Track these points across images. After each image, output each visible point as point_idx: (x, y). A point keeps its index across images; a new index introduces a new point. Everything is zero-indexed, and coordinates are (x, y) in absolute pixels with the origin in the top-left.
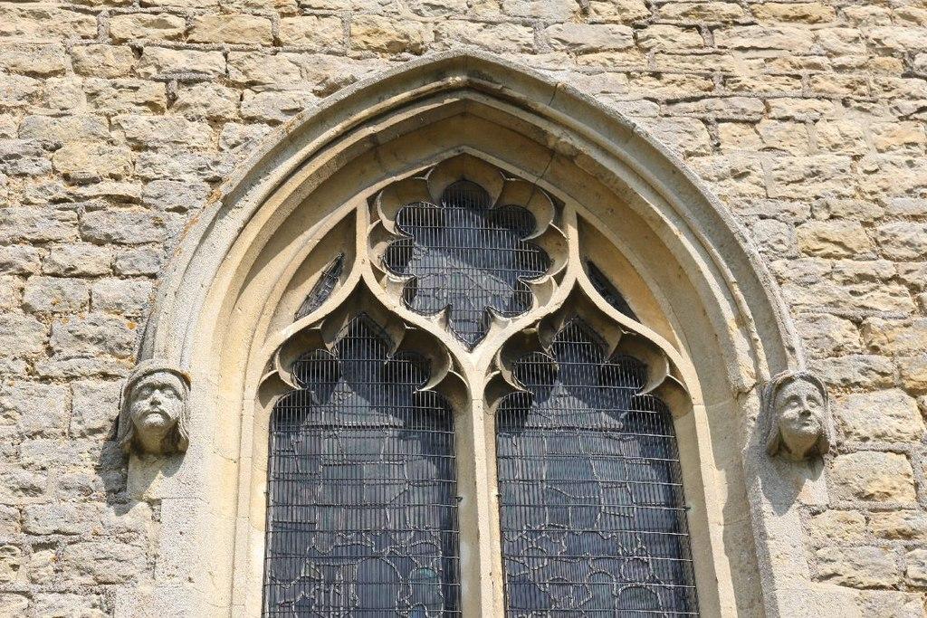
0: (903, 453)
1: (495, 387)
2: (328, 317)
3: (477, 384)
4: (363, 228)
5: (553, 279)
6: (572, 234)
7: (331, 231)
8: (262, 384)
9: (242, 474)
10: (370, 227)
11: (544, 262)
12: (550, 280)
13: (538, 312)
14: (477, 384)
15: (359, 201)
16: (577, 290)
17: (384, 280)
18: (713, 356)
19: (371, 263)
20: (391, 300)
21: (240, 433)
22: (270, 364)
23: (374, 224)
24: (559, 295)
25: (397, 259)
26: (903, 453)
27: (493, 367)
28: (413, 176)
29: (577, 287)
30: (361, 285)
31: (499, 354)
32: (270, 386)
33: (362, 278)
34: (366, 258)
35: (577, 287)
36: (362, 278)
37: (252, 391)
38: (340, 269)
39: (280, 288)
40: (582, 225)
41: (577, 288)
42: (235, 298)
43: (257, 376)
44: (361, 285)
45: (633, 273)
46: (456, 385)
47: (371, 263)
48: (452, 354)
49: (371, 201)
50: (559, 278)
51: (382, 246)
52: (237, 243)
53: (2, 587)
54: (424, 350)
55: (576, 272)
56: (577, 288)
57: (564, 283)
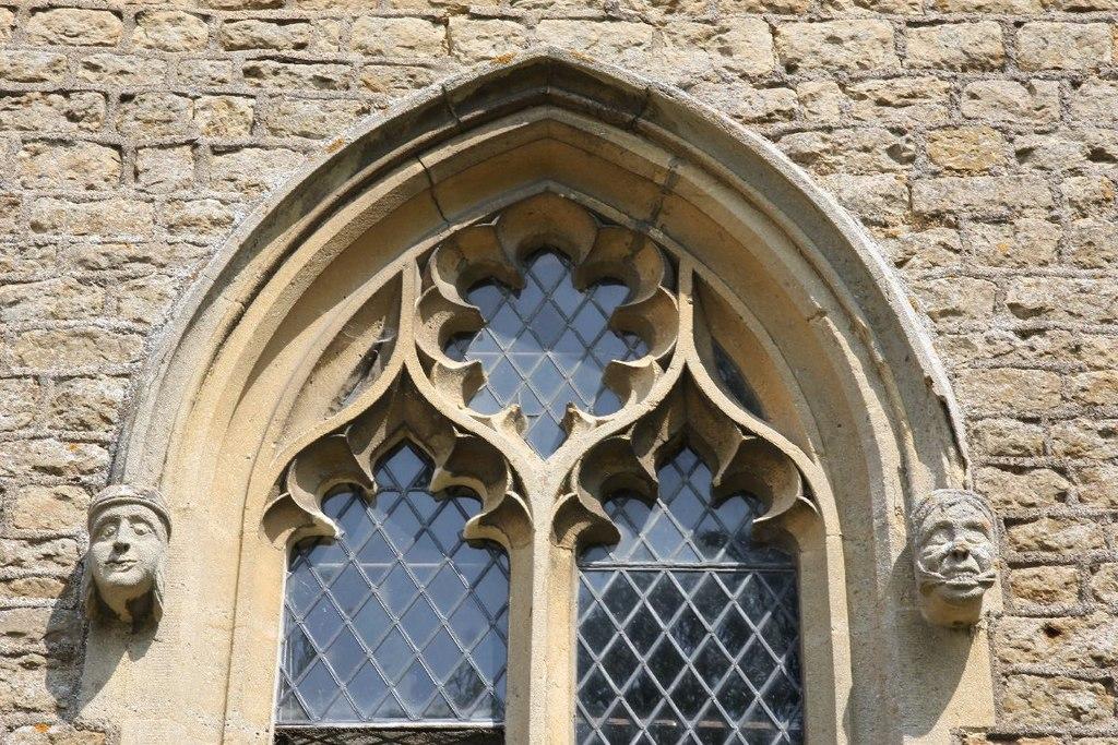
0: (1034, 577)
1: (569, 513)
3: (543, 509)
6: (685, 307)
7: (361, 310)
9: (222, 701)
14: (543, 509)
15: (406, 261)
19: (417, 348)
20: (445, 398)
21: (241, 542)
22: (282, 483)
24: (663, 385)
25: (456, 337)
26: (1034, 577)
27: (566, 487)
29: (686, 373)
30: (404, 376)
32: (281, 512)
33: (404, 366)
35: (686, 373)
36: (404, 366)
40: (701, 293)
41: (686, 375)
43: (259, 506)
44: (404, 376)
45: (778, 374)
46: (513, 514)
47: (417, 348)
48: (512, 468)
49: (423, 262)
50: (665, 363)
51: (440, 319)
53: (3, 276)
54: (481, 460)
55: (686, 350)
56: (686, 375)
57: (690, 275)
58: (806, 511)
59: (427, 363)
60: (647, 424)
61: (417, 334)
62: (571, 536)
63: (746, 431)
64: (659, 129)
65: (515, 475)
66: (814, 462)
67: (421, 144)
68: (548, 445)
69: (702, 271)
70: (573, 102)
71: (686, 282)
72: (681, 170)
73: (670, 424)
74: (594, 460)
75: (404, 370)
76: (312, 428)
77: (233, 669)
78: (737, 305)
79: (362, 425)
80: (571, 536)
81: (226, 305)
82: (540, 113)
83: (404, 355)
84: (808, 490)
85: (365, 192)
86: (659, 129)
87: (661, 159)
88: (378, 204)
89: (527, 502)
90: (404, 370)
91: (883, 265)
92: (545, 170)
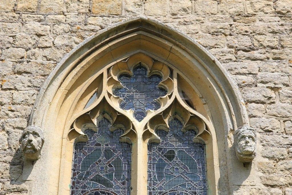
1: (146, 134)
2: (91, 111)
4: (105, 80)
5: (168, 96)
6: (175, 82)
8: (69, 133)
10: (108, 79)
11: (164, 91)
12: (167, 96)
13: (163, 108)
15: (104, 70)
16: (176, 100)
17: (112, 97)
18: (219, 122)
19: (107, 91)
20: (115, 104)
22: (72, 127)
23: (109, 78)
24: (170, 102)
25: (117, 91)
28: (122, 61)
29: (176, 99)
31: (148, 124)
32: (73, 133)
33: (103, 73)
34: (107, 89)
35: (176, 99)
36: (103, 73)
37: (66, 135)
38: (99, 93)
39: (77, 101)
40: (179, 78)
41: (176, 99)
42: (61, 104)
43: (68, 130)
45: (197, 97)
46: (133, 134)
47: (107, 91)
49: (108, 70)
50: (170, 97)
52: (66, 79)
54: (124, 120)
55: (176, 93)
56: (176, 99)
58: (206, 133)
59: (109, 95)
60: (166, 112)
61: (107, 89)
62: (147, 141)
63: (191, 113)
64: (171, 39)
65: (133, 125)
66: (209, 121)
67: (119, 35)
68: (140, 119)
69: (180, 74)
70: (151, 31)
71: (175, 75)
72: (173, 47)
73: (172, 113)
74: (153, 121)
75: (104, 97)
76: (81, 112)
77: (61, 172)
78: (187, 80)
79: (93, 112)
80: (147, 141)
81: (56, 83)
82: (140, 32)
83: (104, 94)
84: (207, 128)
85: (85, 59)
86: (171, 39)
87: (170, 45)
88: (88, 63)
89: (135, 130)
90: (104, 97)
91: (225, 70)
92: (140, 47)
